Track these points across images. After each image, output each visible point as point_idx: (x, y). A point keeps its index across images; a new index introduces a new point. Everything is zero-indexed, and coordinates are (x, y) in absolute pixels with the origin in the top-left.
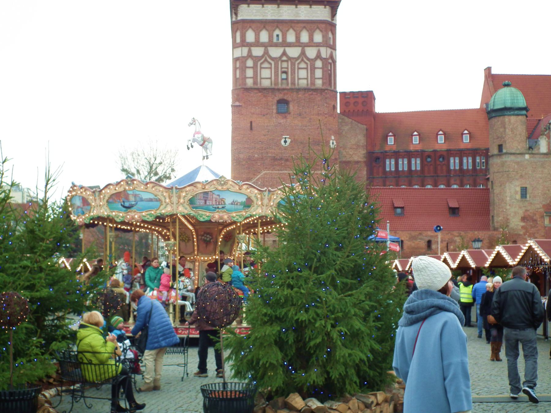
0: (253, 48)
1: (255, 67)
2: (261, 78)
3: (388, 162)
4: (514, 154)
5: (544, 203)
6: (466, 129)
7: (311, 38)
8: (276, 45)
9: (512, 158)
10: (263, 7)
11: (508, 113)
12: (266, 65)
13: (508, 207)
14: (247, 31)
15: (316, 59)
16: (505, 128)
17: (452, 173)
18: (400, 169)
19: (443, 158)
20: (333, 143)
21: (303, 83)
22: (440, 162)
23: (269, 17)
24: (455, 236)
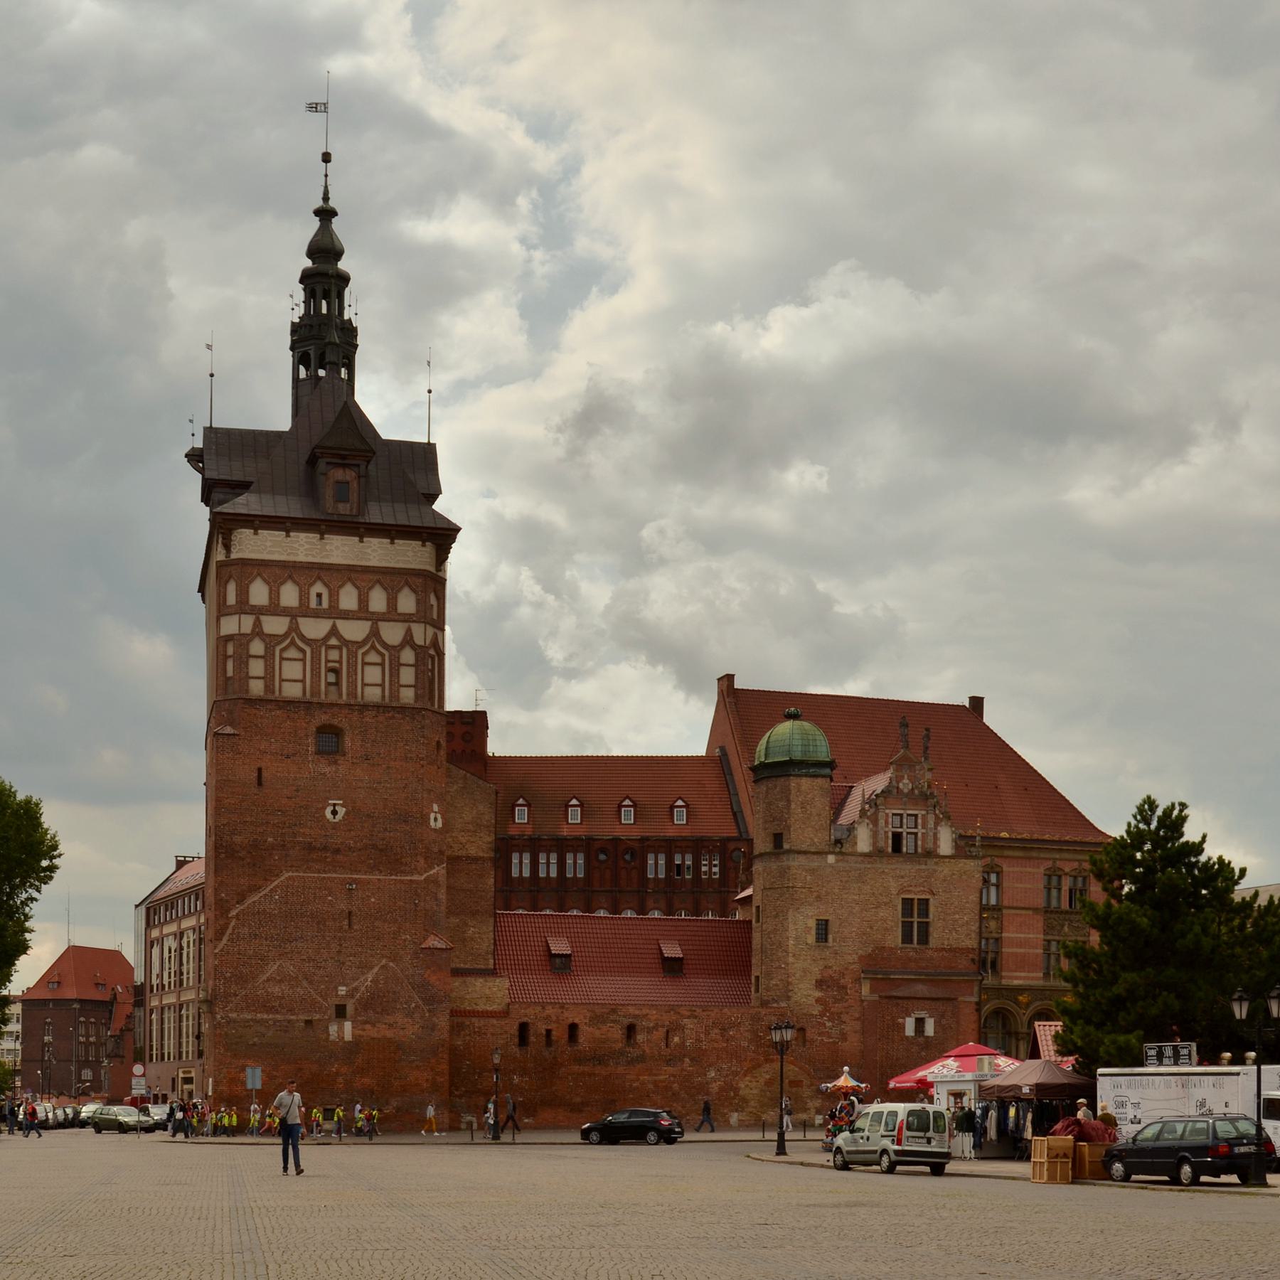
0: (263, 618)
1: (268, 657)
2: (282, 680)
3: (515, 860)
4: (805, 853)
6: (627, 797)
7: (392, 602)
8: (317, 614)
9: (801, 860)
10: (288, 536)
11: (796, 771)
12: (293, 653)
13: (791, 959)
14: (251, 582)
15: (402, 646)
16: (789, 801)
17: (651, 885)
18: (542, 874)
19: (632, 855)
20: (436, 822)
21: (373, 694)
23: (302, 558)
24: (683, 1016)
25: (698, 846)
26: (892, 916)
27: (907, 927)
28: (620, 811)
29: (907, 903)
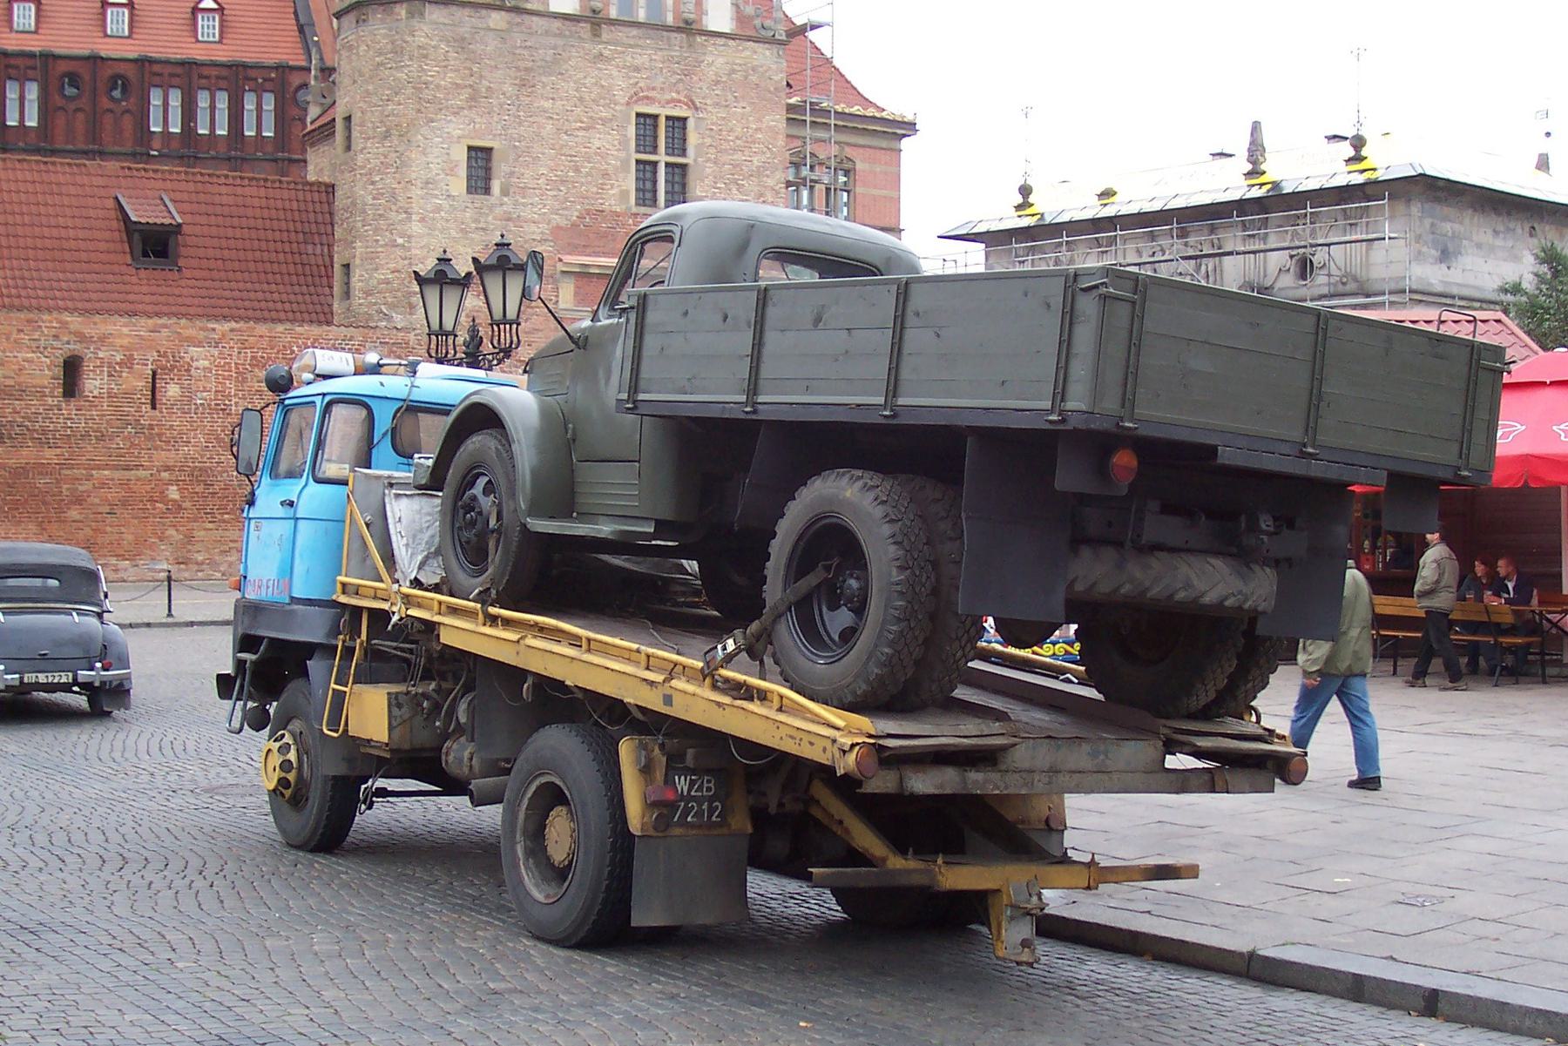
5: (557, 220)
13: (416, 228)
17: (156, 144)
22: (113, 99)
25: (236, 78)
26: (616, 148)
27: (646, 169)
28: (104, 15)
29: (647, 122)
